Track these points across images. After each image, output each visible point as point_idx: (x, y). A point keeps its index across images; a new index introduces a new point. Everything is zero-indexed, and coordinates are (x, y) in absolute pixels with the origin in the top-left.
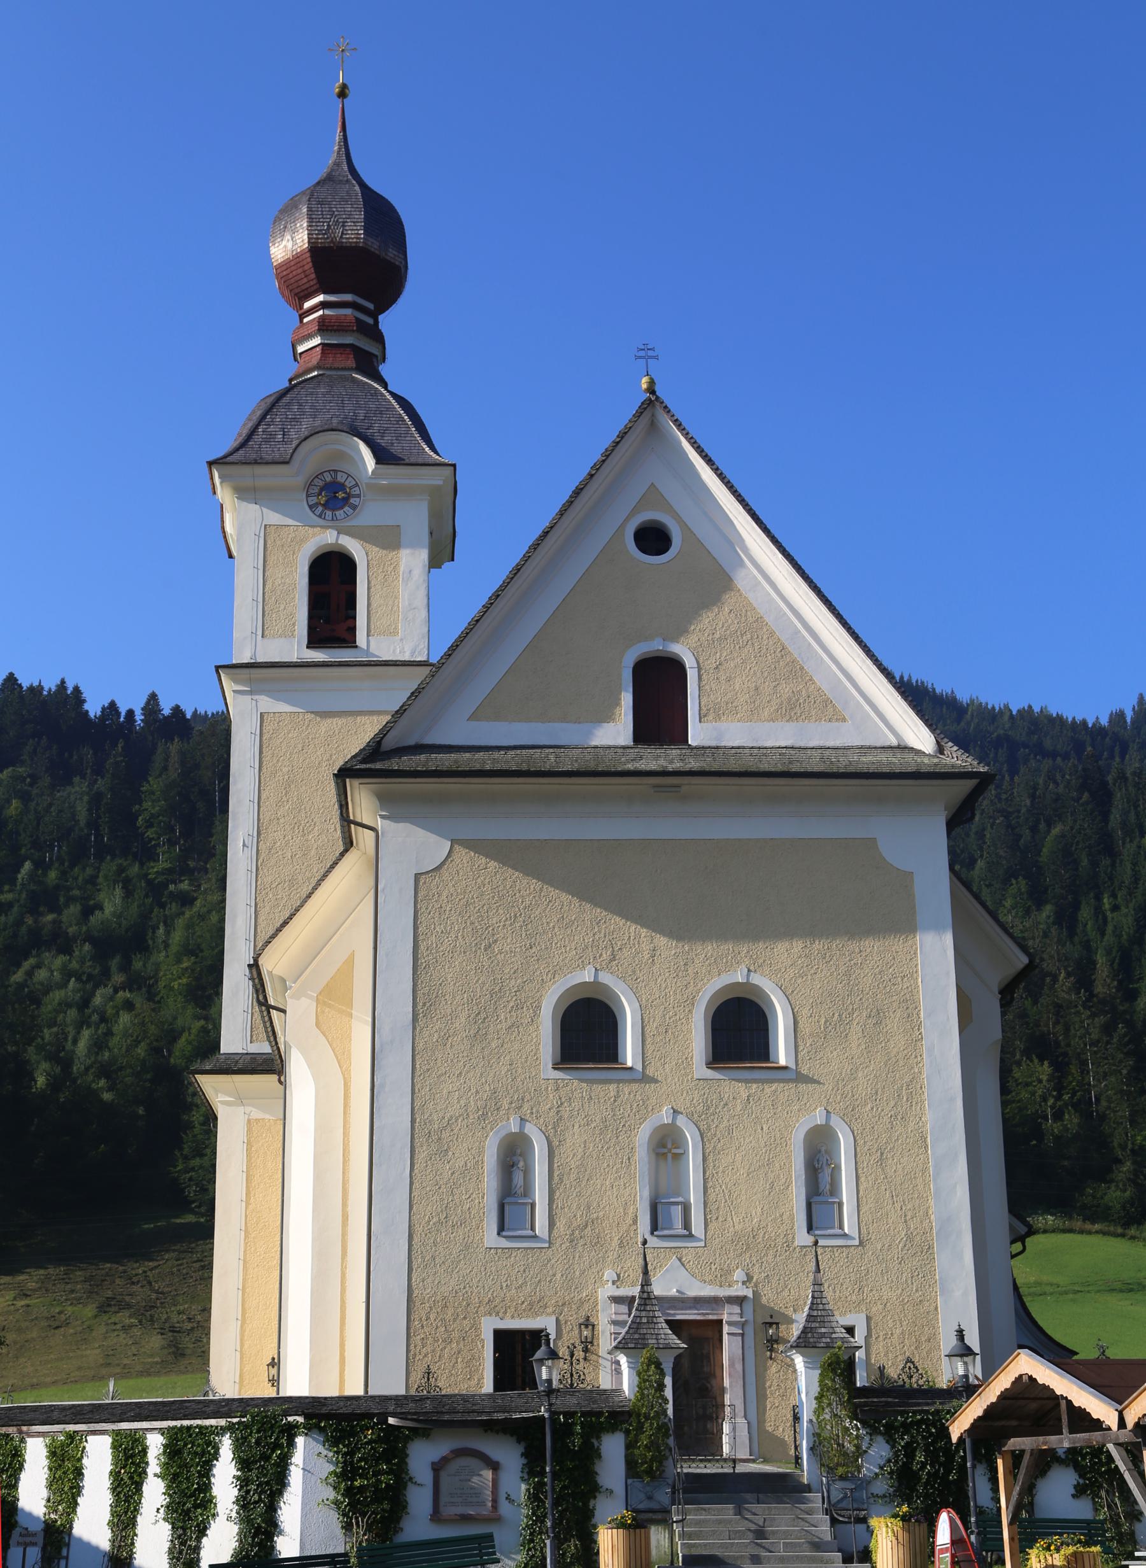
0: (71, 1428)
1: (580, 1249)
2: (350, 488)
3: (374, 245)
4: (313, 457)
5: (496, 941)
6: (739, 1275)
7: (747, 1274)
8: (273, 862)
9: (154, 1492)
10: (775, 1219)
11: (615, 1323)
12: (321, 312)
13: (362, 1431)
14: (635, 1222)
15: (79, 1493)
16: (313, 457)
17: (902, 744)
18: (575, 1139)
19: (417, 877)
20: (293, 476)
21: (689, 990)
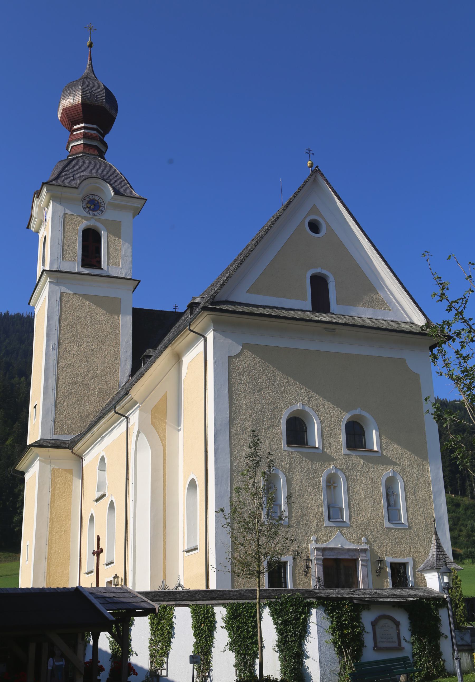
0: (165, 603)
1: (301, 526)
2: (101, 203)
3: (108, 107)
4: (87, 187)
5: (262, 389)
6: (363, 539)
7: (367, 539)
8: (65, 356)
9: (222, 637)
10: (376, 516)
11: (317, 559)
12: (83, 131)
13: (343, 606)
14: (322, 515)
15: (172, 636)
16: (87, 187)
17: (412, 322)
18: (297, 478)
19: (230, 358)
20: (78, 194)
21: (339, 416)
